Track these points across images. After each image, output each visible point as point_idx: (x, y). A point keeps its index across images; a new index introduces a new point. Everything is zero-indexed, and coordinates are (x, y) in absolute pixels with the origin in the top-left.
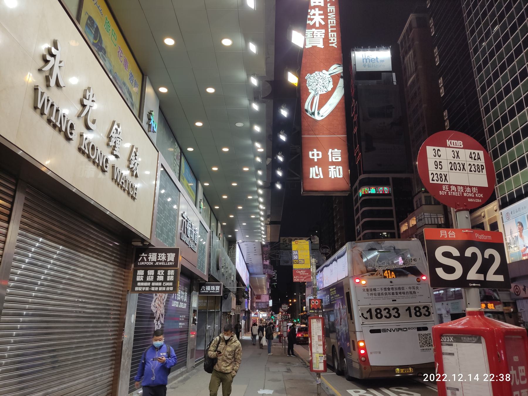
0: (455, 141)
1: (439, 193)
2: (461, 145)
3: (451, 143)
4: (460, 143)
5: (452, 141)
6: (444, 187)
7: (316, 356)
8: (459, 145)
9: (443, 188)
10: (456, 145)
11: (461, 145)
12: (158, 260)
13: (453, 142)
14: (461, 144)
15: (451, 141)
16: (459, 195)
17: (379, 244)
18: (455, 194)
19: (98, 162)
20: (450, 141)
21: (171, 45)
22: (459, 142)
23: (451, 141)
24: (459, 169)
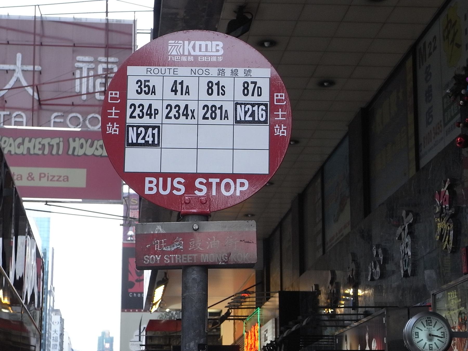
0: (203, 43)
1: (184, 184)
2: (217, 51)
3: (194, 48)
4: (217, 45)
5: (198, 43)
6: (116, 94)
7: (238, 73)
8: (214, 50)
9: (114, 92)
10: (206, 50)
11: (217, 51)
12: (218, 180)
13: (200, 45)
14: (218, 48)
15: (195, 44)
16: (190, 260)
17: (69, 337)
18: (181, 258)
19: (52, 306)
20: (192, 42)
21: (347, 293)
22: (215, 43)
23: (195, 44)
24: (222, 93)
